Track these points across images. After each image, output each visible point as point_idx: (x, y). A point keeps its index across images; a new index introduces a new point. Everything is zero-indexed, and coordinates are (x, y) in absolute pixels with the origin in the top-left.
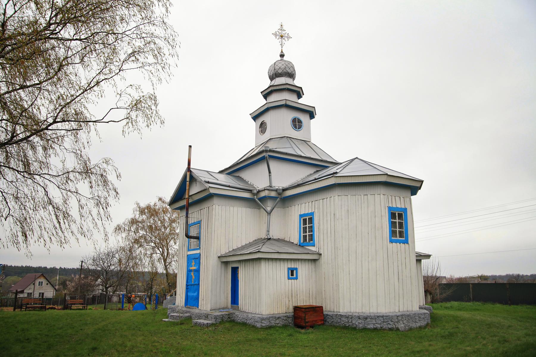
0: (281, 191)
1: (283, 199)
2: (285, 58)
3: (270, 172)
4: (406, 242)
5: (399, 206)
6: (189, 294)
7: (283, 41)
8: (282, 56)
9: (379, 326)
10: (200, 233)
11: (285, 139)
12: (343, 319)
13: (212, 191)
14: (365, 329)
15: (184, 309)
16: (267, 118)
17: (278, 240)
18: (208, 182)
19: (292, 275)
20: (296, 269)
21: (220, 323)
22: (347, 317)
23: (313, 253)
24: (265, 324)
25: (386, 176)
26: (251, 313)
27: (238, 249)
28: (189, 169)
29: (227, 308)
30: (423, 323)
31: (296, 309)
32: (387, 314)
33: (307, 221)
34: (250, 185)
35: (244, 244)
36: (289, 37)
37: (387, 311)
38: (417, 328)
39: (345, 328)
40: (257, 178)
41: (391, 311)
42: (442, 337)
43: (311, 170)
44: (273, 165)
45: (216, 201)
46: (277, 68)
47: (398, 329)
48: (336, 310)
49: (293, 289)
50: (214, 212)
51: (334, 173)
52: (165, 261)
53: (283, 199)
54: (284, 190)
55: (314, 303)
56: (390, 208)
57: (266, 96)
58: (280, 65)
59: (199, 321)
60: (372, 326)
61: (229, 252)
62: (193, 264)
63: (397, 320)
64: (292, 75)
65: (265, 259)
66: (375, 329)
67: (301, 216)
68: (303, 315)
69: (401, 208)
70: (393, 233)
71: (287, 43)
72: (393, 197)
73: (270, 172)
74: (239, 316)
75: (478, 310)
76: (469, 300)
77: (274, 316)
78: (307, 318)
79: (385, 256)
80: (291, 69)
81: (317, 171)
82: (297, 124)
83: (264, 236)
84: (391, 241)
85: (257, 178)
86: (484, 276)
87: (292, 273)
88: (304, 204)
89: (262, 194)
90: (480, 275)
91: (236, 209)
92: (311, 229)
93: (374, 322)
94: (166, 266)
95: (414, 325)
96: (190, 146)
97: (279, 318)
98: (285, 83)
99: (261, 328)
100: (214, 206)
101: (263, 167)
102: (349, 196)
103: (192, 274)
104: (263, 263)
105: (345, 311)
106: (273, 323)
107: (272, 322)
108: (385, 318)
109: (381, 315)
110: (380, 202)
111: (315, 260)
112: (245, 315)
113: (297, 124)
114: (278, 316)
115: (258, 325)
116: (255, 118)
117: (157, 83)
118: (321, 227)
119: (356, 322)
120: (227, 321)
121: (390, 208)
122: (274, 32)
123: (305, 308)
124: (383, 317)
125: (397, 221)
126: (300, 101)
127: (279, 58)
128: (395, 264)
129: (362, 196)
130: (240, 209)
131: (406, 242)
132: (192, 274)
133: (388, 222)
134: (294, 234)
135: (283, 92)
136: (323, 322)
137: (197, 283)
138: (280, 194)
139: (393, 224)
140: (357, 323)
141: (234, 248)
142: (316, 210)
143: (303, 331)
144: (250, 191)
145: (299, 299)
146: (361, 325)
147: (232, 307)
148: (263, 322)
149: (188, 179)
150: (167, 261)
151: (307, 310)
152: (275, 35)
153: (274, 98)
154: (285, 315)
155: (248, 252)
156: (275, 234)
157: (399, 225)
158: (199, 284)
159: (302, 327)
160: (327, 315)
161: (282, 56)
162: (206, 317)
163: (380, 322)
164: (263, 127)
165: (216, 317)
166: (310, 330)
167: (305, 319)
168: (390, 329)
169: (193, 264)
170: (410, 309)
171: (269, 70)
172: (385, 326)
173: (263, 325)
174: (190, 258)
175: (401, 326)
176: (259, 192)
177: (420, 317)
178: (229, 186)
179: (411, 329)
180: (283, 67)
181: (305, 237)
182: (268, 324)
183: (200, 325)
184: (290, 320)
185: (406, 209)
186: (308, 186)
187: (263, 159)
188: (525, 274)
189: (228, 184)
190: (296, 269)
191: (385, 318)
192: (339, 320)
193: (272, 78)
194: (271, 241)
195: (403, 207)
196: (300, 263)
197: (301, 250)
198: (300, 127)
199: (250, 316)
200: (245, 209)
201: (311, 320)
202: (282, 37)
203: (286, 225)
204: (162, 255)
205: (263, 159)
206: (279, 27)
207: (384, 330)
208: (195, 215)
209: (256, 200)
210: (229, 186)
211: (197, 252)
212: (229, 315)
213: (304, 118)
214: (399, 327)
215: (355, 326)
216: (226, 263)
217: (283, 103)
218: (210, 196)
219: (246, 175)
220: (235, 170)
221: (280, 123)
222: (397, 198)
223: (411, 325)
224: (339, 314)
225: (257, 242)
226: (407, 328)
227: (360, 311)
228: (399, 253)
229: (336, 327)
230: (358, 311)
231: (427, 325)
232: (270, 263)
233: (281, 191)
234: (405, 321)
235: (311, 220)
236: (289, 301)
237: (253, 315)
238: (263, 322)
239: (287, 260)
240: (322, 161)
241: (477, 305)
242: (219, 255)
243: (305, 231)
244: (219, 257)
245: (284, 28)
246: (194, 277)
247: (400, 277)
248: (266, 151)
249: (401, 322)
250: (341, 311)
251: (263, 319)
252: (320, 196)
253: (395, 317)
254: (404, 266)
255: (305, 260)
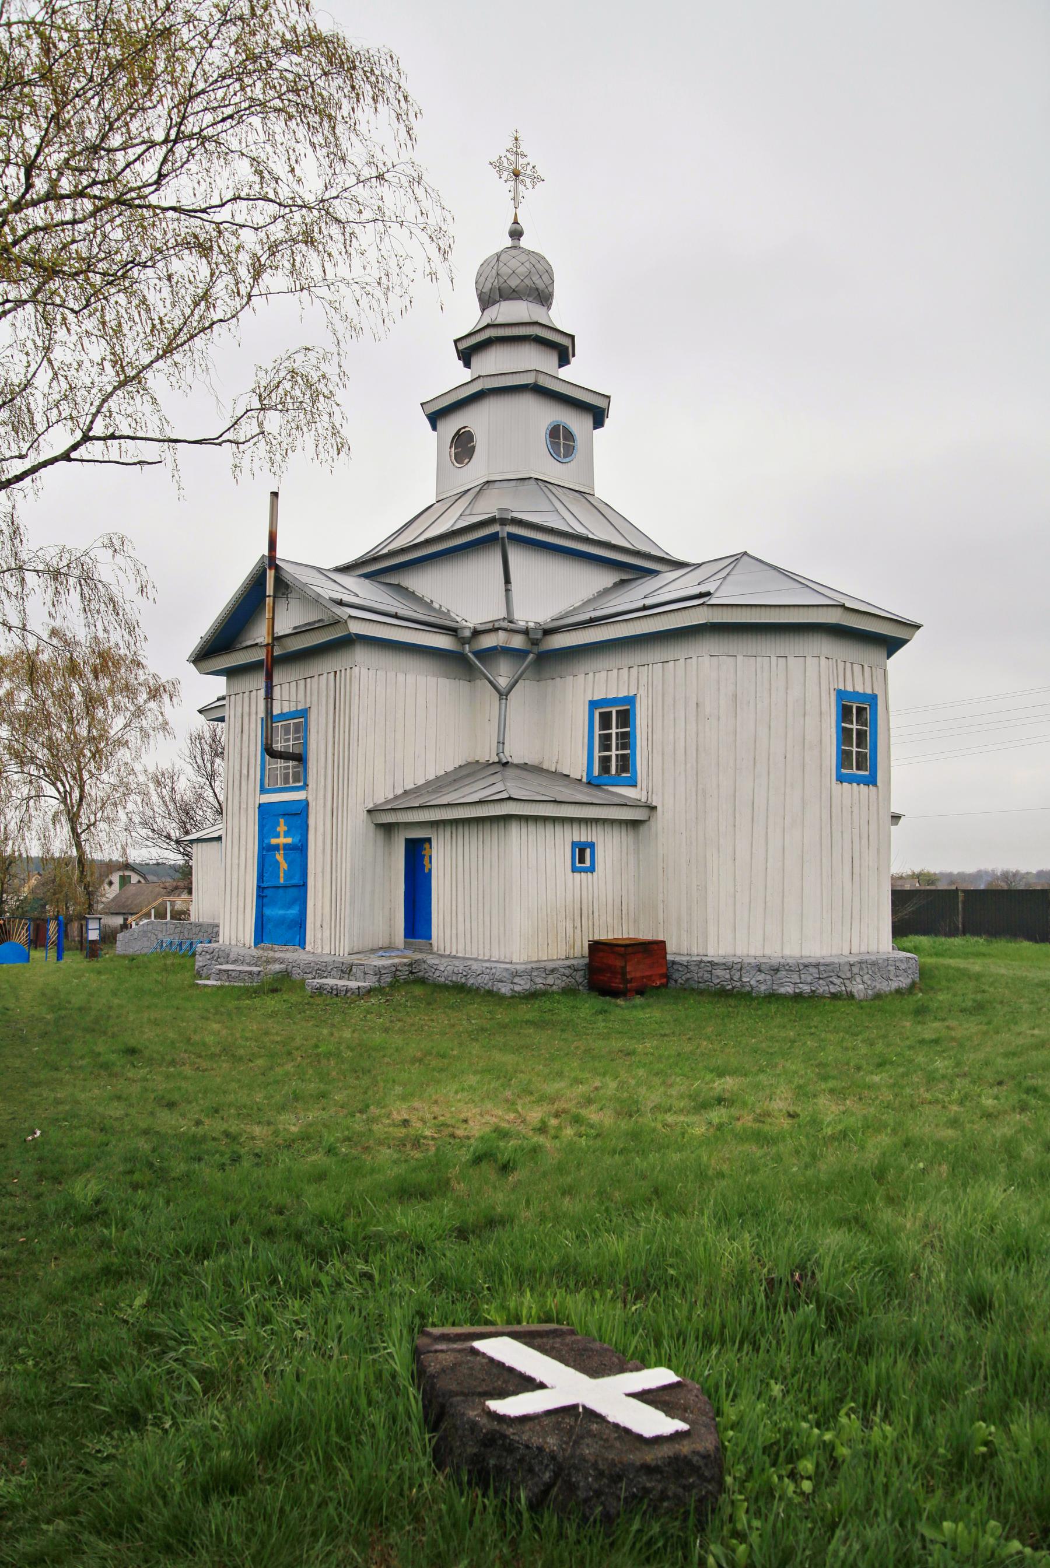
0: (539, 636)
1: (543, 654)
2: (524, 242)
3: (507, 581)
4: (871, 781)
5: (859, 689)
6: (268, 912)
7: (521, 187)
8: (516, 234)
9: (806, 989)
10: (305, 744)
11: (533, 482)
12: (719, 972)
13: (355, 628)
14: (772, 997)
15: (255, 952)
16: (476, 420)
17: (524, 767)
18: (341, 603)
19: (582, 860)
20: (592, 845)
21: (392, 985)
22: (728, 967)
23: (634, 805)
24: (522, 985)
25: (840, 610)
26: (476, 960)
27: (417, 790)
28: (271, 560)
29: (389, 948)
30: (904, 982)
31: (596, 947)
32: (828, 960)
33: (615, 721)
34: (439, 611)
35: (432, 777)
36: (536, 179)
37: (825, 953)
38: (891, 992)
39: (723, 994)
40: (467, 594)
41: (834, 952)
42: (963, 1011)
43: (606, 579)
44: (518, 558)
45: (361, 656)
46: (505, 271)
47: (851, 996)
48: (695, 951)
49: (584, 897)
50: (355, 686)
51: (701, 595)
52: (73, 819)
53: (543, 654)
54: (548, 632)
55: (645, 934)
56: (841, 694)
57: (466, 356)
58: (514, 264)
59: (324, 981)
60: (789, 989)
61: (396, 798)
62: (282, 828)
63: (849, 975)
64: (544, 298)
65: (520, 818)
66: (798, 997)
67: (593, 704)
68: (619, 963)
69: (865, 694)
70: (844, 758)
71: (529, 194)
72: (848, 665)
73: (507, 581)
74: (443, 970)
75: (984, 955)
76: (952, 933)
77: (542, 965)
78: (621, 971)
79: (826, 816)
80: (545, 277)
81: (623, 582)
82: (561, 441)
83: (487, 753)
84: (841, 779)
85: (467, 594)
86: (928, 874)
87: (582, 853)
88: (604, 674)
89: (488, 642)
90: (917, 870)
91: (411, 678)
92: (626, 740)
93: (795, 978)
94: (76, 835)
95: (885, 987)
96: (275, 495)
97: (553, 971)
98: (527, 320)
99: (512, 997)
100: (356, 669)
101: (489, 564)
102: (740, 658)
103: (279, 857)
104: (514, 829)
105: (722, 952)
106: (540, 983)
107: (539, 980)
108: (822, 968)
109: (813, 961)
110: (816, 675)
111: (635, 824)
112: (460, 966)
113: (561, 441)
114: (550, 966)
115: (505, 989)
116: (435, 418)
117: (348, 337)
118: (658, 736)
119: (751, 979)
120: (407, 982)
121: (841, 694)
122: (495, 159)
123: (626, 946)
124: (817, 966)
125: (855, 749)
126: (564, 373)
127: (508, 242)
128: (847, 836)
129: (774, 659)
130: (422, 679)
131: (871, 781)
132: (279, 857)
133: (834, 730)
134: (573, 753)
135: (518, 348)
136: (664, 980)
137: (295, 881)
138: (535, 642)
139: (845, 735)
140: (753, 982)
141: (408, 788)
142: (642, 692)
143: (620, 1002)
144: (452, 631)
145: (596, 923)
146: (763, 988)
147: (407, 946)
148: (516, 980)
149: (270, 590)
150: (83, 820)
151: (630, 949)
152: (498, 166)
153: (495, 363)
154: (568, 963)
155: (475, 798)
156: (518, 751)
157: (858, 737)
158: (305, 885)
159: (615, 994)
160: (674, 963)
161: (516, 234)
162: (347, 971)
163: (809, 979)
164: (463, 446)
165: (378, 972)
166: (638, 1000)
167: (624, 974)
168: (835, 996)
169: (282, 828)
170: (873, 948)
171: (479, 275)
172: (822, 988)
173: (517, 988)
174: (267, 815)
175: (858, 988)
176: (476, 633)
177: (897, 968)
178: (396, 616)
179: (878, 996)
180: (522, 270)
181: (605, 761)
182: (527, 987)
183: (335, 992)
184: (579, 976)
185: (874, 697)
186: (623, 625)
187: (493, 538)
188: (1023, 870)
189: (392, 610)
190: (592, 845)
191: (821, 969)
192: (707, 976)
193: (486, 301)
194: (510, 772)
195: (869, 691)
196: (600, 828)
197: (597, 796)
198: (569, 451)
199: (475, 966)
200: (447, 681)
201: (638, 974)
202: (516, 174)
203: (555, 727)
204: (64, 801)
205: (492, 539)
206: (510, 144)
207: (821, 997)
208: (291, 691)
209: (464, 656)
210: (396, 616)
211: (299, 796)
212: (411, 965)
213: (578, 423)
214: (855, 991)
215: (748, 989)
216: (388, 829)
217: (529, 379)
218: (348, 642)
219: (429, 584)
220: (382, 567)
221: (509, 436)
222: (857, 668)
223: (878, 986)
224: (705, 959)
225: (470, 771)
226: (870, 992)
227: (759, 953)
228: (856, 810)
229: (701, 993)
230: (752, 953)
231: (913, 985)
232: (532, 828)
233: (539, 636)
234: (866, 978)
235: (626, 718)
236: (575, 928)
237: (487, 965)
238: (516, 980)
239: (572, 820)
240: (638, 554)
241: (978, 942)
242: (370, 806)
243: (605, 746)
244: (369, 811)
245: (523, 148)
246: (284, 866)
247: (856, 870)
248: (503, 522)
249: (858, 979)
250: (711, 952)
251: (516, 974)
252: (655, 654)
253: (847, 967)
254: (865, 841)
255: (612, 822)
